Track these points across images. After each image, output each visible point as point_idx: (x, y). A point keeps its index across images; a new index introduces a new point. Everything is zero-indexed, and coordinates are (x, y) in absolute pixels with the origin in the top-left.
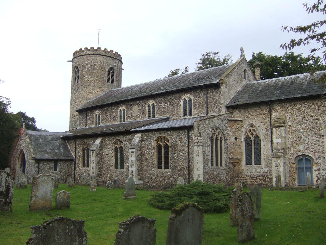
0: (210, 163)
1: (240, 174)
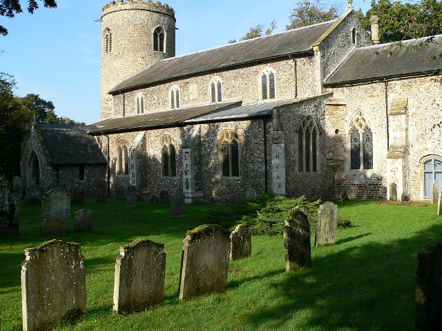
0: (297, 168)
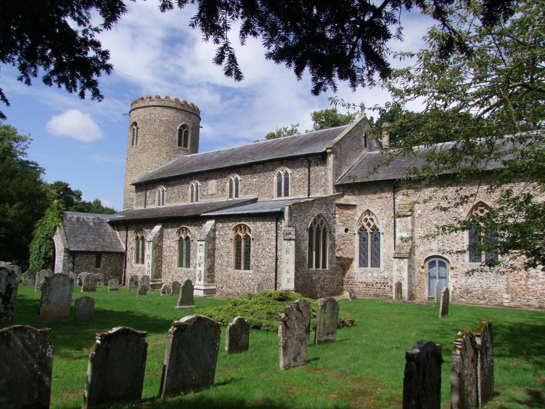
1: (351, 279)
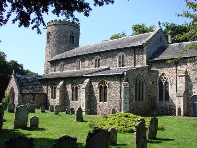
0: (134, 99)
